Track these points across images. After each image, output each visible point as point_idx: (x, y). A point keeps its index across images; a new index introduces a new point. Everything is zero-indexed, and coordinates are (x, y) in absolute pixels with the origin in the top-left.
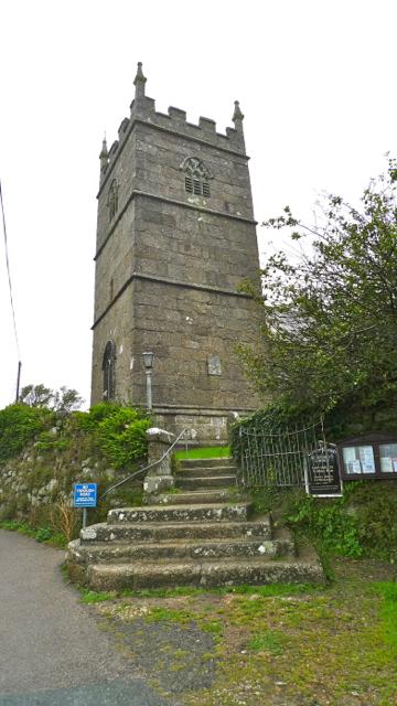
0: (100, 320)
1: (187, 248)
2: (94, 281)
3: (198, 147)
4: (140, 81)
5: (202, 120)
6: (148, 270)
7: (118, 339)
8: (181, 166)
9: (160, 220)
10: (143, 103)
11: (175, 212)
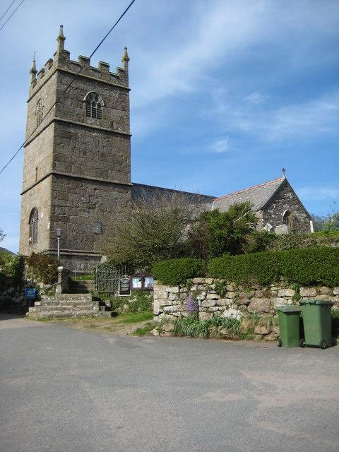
1: (85, 153)
4: (62, 39)
9: (69, 136)
11: (80, 132)
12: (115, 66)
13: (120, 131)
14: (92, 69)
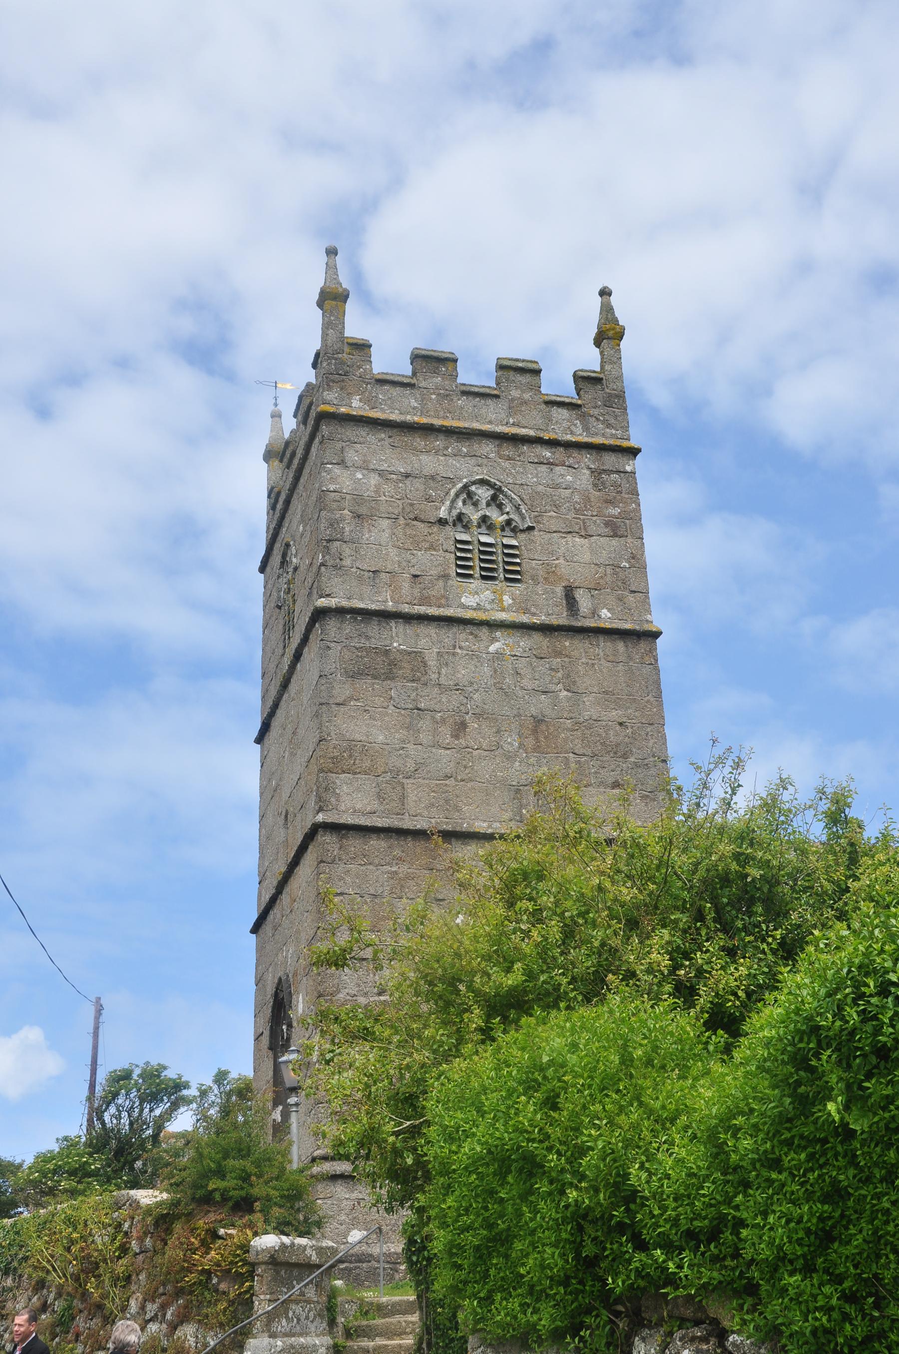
0: (276, 706)
3: (488, 448)
5: (505, 368)
6: (354, 802)
7: (295, 974)
8: (443, 513)
9: (384, 668)
11: (428, 641)
13: (606, 617)
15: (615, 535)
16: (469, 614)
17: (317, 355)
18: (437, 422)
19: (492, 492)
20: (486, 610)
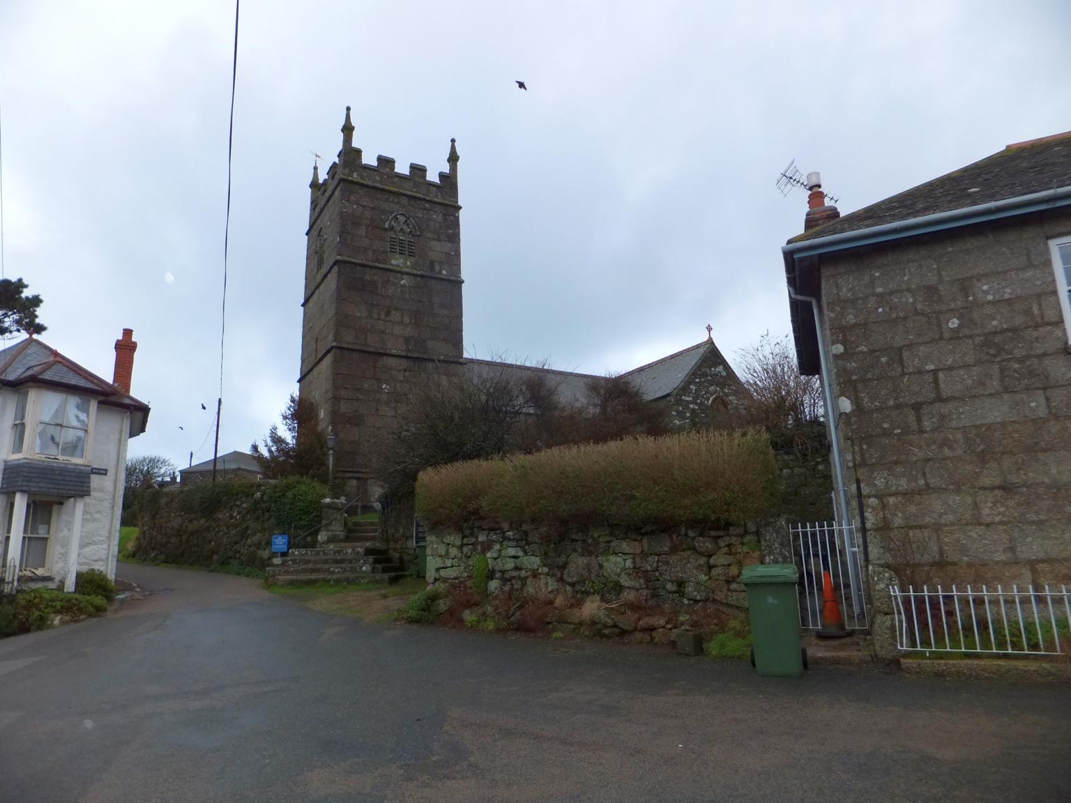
2: (301, 352)
4: (348, 129)
6: (349, 339)
8: (386, 225)
10: (350, 155)
12: (435, 170)
14: (398, 176)
15: (450, 241)
16: (394, 268)
17: (340, 152)
18: (387, 188)
19: (405, 219)
20: (400, 267)
